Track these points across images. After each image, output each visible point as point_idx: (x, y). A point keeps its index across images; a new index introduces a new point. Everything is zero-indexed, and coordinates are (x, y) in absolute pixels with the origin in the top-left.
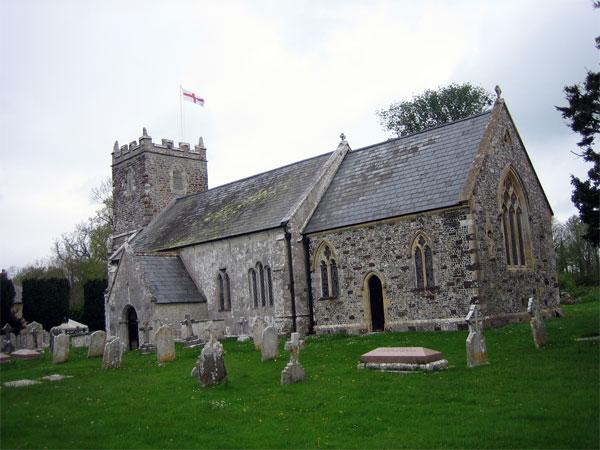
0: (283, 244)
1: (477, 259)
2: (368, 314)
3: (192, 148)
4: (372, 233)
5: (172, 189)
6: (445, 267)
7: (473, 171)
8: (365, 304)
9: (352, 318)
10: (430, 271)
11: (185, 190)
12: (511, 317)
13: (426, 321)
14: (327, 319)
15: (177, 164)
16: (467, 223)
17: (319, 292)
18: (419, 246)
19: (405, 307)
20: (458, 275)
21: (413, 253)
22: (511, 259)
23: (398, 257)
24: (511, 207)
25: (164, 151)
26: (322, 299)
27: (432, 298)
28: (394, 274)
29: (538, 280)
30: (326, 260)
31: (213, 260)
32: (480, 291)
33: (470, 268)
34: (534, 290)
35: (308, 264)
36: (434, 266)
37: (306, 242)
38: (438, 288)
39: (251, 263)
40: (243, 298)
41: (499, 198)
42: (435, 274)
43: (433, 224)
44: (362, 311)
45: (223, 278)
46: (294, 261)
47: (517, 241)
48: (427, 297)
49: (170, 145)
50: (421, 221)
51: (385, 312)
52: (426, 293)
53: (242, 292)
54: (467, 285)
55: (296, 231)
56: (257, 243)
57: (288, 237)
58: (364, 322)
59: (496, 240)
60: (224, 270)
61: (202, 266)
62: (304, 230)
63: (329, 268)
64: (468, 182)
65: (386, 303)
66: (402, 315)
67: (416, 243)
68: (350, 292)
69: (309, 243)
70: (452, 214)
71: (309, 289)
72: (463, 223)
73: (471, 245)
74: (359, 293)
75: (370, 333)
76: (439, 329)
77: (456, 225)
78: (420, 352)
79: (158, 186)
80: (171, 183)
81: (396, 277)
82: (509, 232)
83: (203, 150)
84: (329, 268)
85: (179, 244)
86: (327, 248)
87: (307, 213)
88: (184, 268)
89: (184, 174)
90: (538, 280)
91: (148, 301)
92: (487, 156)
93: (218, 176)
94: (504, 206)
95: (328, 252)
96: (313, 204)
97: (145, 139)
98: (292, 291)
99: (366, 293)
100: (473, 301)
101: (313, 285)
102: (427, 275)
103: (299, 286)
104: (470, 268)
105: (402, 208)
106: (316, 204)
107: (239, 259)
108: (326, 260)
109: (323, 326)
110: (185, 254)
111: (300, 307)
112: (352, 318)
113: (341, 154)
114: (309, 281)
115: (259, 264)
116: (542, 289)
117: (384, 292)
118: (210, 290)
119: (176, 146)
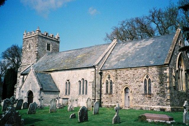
4: (128, 72)
6: (156, 87)
10: (150, 88)
14: (107, 102)
18: (146, 78)
21: (144, 81)
25: (45, 36)
36: (152, 86)
38: (153, 94)
43: (153, 71)
45: (68, 83)
52: (148, 96)
60: (68, 80)
67: (145, 77)
72: (165, 72)
80: (46, 48)
81: (136, 89)
86: (109, 76)
95: (109, 78)
102: (149, 89)
103: (98, 89)
111: (97, 96)
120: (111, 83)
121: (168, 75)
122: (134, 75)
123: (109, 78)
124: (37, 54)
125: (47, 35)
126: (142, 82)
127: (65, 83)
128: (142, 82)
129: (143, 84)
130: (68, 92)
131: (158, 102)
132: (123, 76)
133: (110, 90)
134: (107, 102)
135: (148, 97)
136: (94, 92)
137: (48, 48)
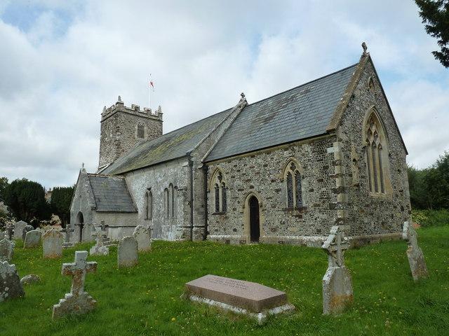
0: (187, 169)
1: (342, 182)
2: (247, 228)
3: (153, 113)
4: (253, 161)
5: (136, 137)
6: (312, 190)
7: (341, 106)
8: (245, 219)
9: (235, 230)
10: (299, 193)
11: (146, 138)
12: (373, 239)
13: (294, 237)
14: (216, 230)
15: (141, 121)
16: (335, 149)
17: (212, 209)
18: (291, 171)
19: (277, 223)
20: (324, 198)
21: (285, 177)
22: (373, 187)
23: (273, 181)
24: (374, 143)
25: (132, 113)
26: (213, 214)
27: (300, 217)
28: (270, 195)
29: (395, 207)
30: (219, 183)
31: (144, 182)
32: (344, 213)
33: (335, 191)
34: (392, 215)
35: (206, 186)
36: (303, 189)
37: (205, 169)
38: (305, 208)
39: (166, 185)
40: (160, 211)
41: (363, 132)
42: (303, 196)
43: (303, 152)
44: (243, 225)
45: (149, 194)
46: (194, 183)
47: (378, 172)
48: (296, 216)
49: (137, 108)
50: (293, 150)
51: (261, 228)
52: (295, 213)
53: (159, 206)
54: (332, 207)
55: (198, 159)
56: (171, 170)
57: (191, 164)
58: (244, 234)
59: (359, 168)
60: (149, 189)
61: (137, 186)
62: (205, 159)
63: (220, 190)
64: (336, 114)
65: (262, 219)
66: (274, 230)
67: (288, 169)
68: (234, 209)
69: (207, 169)
70: (321, 140)
71: (205, 206)
72: (330, 150)
73: (337, 170)
74: (241, 210)
75: (249, 243)
76: (306, 245)
77: (323, 152)
78: (256, 291)
79: (126, 135)
80: (136, 133)
81: (271, 198)
82: (371, 163)
83: (161, 114)
84: (220, 190)
85: (125, 171)
86: (220, 173)
87: (208, 147)
88: (126, 188)
89: (145, 128)
90: (395, 207)
91: (90, 209)
92: (353, 96)
93: (168, 128)
94: (367, 140)
95: (220, 178)
96: (214, 141)
97: (120, 103)
98: (191, 207)
99: (247, 210)
100: (337, 222)
101: (208, 202)
102: (297, 196)
103: (197, 203)
104: (335, 191)
105: (278, 139)
106: (216, 141)
107: (160, 179)
108: (219, 183)
109: (214, 236)
110: (129, 179)
111: (196, 219)
112: (235, 230)
113: (240, 107)
114: (206, 199)
115: (171, 184)
116: (399, 215)
117: (260, 210)
118: (140, 203)
119: (142, 110)
120: (224, 189)
121: (336, 158)
122: (266, 166)
123: (220, 178)
124: (117, 145)
125: (136, 110)
126: (282, 182)
127: (144, 194)
128: (282, 182)
129: (284, 185)
130: (148, 209)
131: (318, 226)
132: (244, 172)
133: (223, 203)
134: (216, 230)
135: (296, 216)
136: (189, 209)
137: (141, 134)
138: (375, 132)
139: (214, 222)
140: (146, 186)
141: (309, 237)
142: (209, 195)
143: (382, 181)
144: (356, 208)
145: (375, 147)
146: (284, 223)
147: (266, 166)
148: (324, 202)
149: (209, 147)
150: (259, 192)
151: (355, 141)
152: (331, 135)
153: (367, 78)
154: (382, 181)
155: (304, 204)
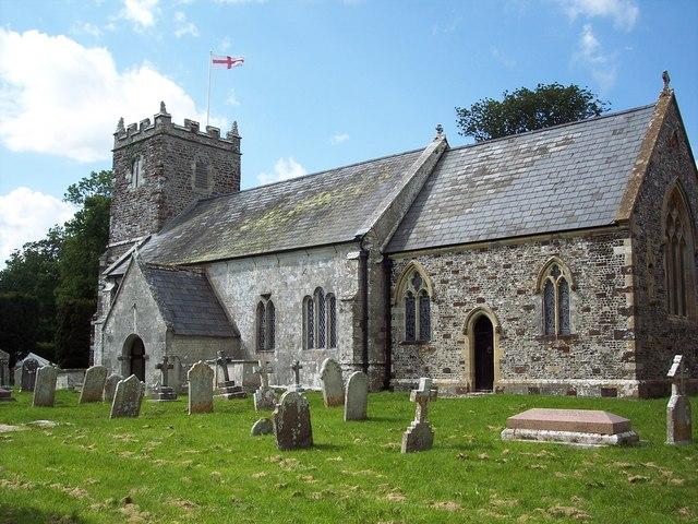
0: (356, 265)
3: (223, 136)
4: (485, 257)
5: (193, 186)
6: (588, 310)
8: (465, 352)
9: (447, 371)
10: (563, 314)
14: (410, 371)
15: (201, 154)
18: (551, 278)
19: (526, 360)
23: (520, 292)
24: (675, 237)
25: (186, 136)
27: (566, 350)
30: (413, 291)
31: (252, 282)
38: (576, 336)
42: (572, 318)
45: (266, 309)
48: (559, 349)
49: (195, 127)
52: (558, 343)
57: (364, 258)
58: (464, 377)
61: (237, 288)
62: (386, 247)
64: (627, 195)
65: (498, 353)
68: (447, 336)
69: (392, 266)
71: (388, 329)
72: (617, 250)
76: (574, 393)
77: (607, 252)
81: (516, 319)
83: (237, 139)
96: (398, 214)
97: (164, 117)
103: (374, 324)
106: (402, 215)
108: (413, 291)
112: (447, 371)
114: (388, 317)
117: (496, 338)
118: (245, 324)
124: (159, 202)
129: (538, 300)
135: (559, 349)
138: (677, 220)
139: (406, 357)
140: (257, 293)
141: (580, 381)
142: (394, 311)
143: (683, 298)
144: (650, 339)
145: (677, 242)
146: (539, 359)
147: (509, 266)
148: (606, 328)
149: (392, 225)
150: (495, 309)
151: (652, 237)
152: (622, 227)
153: (670, 131)
154: (683, 298)
155: (573, 331)
